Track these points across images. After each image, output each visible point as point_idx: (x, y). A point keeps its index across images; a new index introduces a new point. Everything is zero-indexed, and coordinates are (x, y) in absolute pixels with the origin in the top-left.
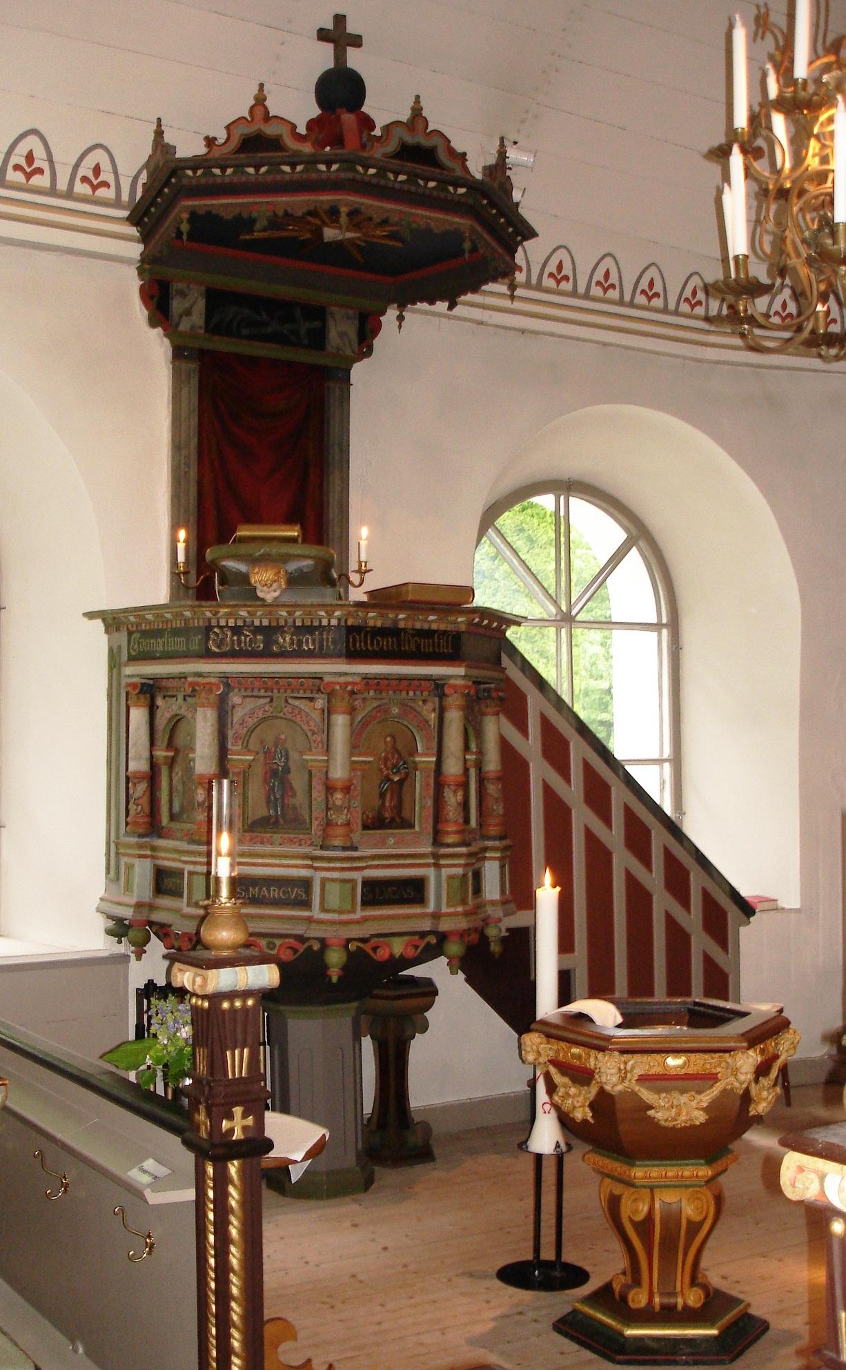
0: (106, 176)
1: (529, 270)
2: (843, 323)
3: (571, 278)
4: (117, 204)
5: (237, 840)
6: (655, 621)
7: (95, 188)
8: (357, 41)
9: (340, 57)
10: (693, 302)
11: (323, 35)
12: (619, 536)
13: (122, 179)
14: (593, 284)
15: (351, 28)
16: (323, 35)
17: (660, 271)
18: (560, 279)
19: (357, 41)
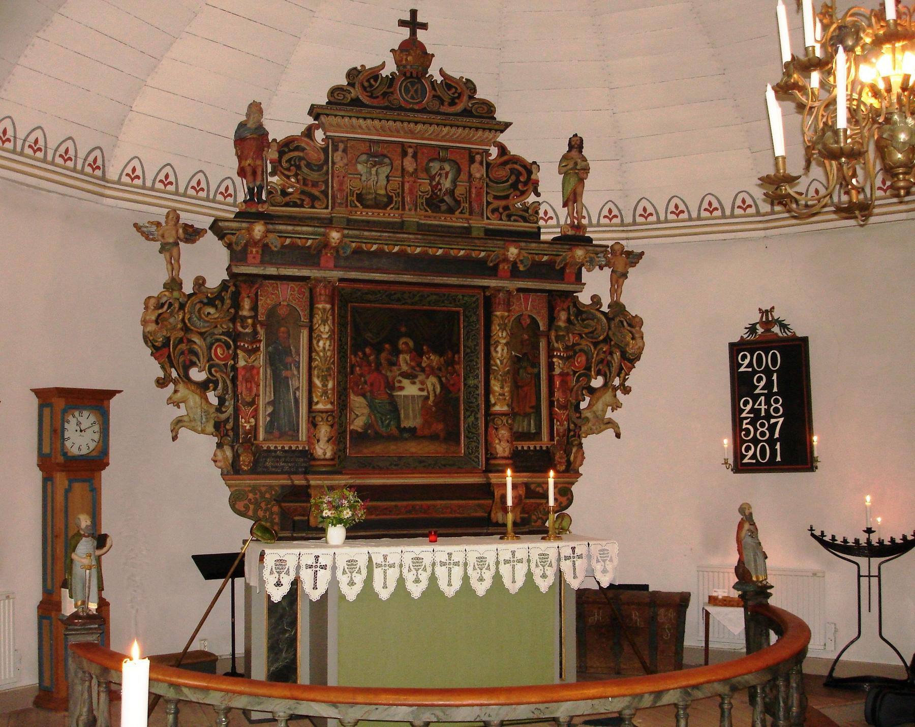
0: (615, 212)
1: (657, 213)
2: (689, 212)
3: (141, 177)
4: (234, 205)
5: (678, 672)
6: (861, 574)
7: (678, 215)
8: (424, 26)
9: (413, 34)
10: (226, 195)
11: (402, 23)
12: (861, 578)
13: (49, 150)
14: (189, 187)
15: (420, 19)
16: (402, 23)
17: (648, 200)
18: (226, 194)
19: (424, 26)
